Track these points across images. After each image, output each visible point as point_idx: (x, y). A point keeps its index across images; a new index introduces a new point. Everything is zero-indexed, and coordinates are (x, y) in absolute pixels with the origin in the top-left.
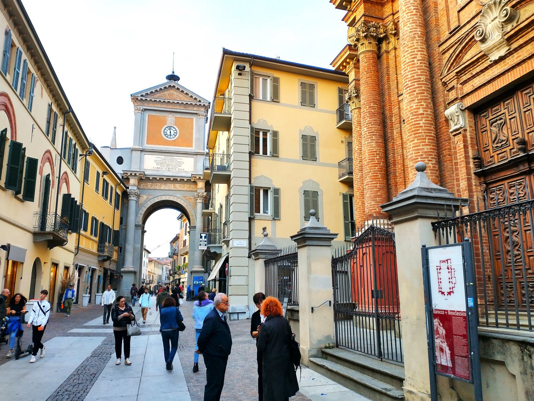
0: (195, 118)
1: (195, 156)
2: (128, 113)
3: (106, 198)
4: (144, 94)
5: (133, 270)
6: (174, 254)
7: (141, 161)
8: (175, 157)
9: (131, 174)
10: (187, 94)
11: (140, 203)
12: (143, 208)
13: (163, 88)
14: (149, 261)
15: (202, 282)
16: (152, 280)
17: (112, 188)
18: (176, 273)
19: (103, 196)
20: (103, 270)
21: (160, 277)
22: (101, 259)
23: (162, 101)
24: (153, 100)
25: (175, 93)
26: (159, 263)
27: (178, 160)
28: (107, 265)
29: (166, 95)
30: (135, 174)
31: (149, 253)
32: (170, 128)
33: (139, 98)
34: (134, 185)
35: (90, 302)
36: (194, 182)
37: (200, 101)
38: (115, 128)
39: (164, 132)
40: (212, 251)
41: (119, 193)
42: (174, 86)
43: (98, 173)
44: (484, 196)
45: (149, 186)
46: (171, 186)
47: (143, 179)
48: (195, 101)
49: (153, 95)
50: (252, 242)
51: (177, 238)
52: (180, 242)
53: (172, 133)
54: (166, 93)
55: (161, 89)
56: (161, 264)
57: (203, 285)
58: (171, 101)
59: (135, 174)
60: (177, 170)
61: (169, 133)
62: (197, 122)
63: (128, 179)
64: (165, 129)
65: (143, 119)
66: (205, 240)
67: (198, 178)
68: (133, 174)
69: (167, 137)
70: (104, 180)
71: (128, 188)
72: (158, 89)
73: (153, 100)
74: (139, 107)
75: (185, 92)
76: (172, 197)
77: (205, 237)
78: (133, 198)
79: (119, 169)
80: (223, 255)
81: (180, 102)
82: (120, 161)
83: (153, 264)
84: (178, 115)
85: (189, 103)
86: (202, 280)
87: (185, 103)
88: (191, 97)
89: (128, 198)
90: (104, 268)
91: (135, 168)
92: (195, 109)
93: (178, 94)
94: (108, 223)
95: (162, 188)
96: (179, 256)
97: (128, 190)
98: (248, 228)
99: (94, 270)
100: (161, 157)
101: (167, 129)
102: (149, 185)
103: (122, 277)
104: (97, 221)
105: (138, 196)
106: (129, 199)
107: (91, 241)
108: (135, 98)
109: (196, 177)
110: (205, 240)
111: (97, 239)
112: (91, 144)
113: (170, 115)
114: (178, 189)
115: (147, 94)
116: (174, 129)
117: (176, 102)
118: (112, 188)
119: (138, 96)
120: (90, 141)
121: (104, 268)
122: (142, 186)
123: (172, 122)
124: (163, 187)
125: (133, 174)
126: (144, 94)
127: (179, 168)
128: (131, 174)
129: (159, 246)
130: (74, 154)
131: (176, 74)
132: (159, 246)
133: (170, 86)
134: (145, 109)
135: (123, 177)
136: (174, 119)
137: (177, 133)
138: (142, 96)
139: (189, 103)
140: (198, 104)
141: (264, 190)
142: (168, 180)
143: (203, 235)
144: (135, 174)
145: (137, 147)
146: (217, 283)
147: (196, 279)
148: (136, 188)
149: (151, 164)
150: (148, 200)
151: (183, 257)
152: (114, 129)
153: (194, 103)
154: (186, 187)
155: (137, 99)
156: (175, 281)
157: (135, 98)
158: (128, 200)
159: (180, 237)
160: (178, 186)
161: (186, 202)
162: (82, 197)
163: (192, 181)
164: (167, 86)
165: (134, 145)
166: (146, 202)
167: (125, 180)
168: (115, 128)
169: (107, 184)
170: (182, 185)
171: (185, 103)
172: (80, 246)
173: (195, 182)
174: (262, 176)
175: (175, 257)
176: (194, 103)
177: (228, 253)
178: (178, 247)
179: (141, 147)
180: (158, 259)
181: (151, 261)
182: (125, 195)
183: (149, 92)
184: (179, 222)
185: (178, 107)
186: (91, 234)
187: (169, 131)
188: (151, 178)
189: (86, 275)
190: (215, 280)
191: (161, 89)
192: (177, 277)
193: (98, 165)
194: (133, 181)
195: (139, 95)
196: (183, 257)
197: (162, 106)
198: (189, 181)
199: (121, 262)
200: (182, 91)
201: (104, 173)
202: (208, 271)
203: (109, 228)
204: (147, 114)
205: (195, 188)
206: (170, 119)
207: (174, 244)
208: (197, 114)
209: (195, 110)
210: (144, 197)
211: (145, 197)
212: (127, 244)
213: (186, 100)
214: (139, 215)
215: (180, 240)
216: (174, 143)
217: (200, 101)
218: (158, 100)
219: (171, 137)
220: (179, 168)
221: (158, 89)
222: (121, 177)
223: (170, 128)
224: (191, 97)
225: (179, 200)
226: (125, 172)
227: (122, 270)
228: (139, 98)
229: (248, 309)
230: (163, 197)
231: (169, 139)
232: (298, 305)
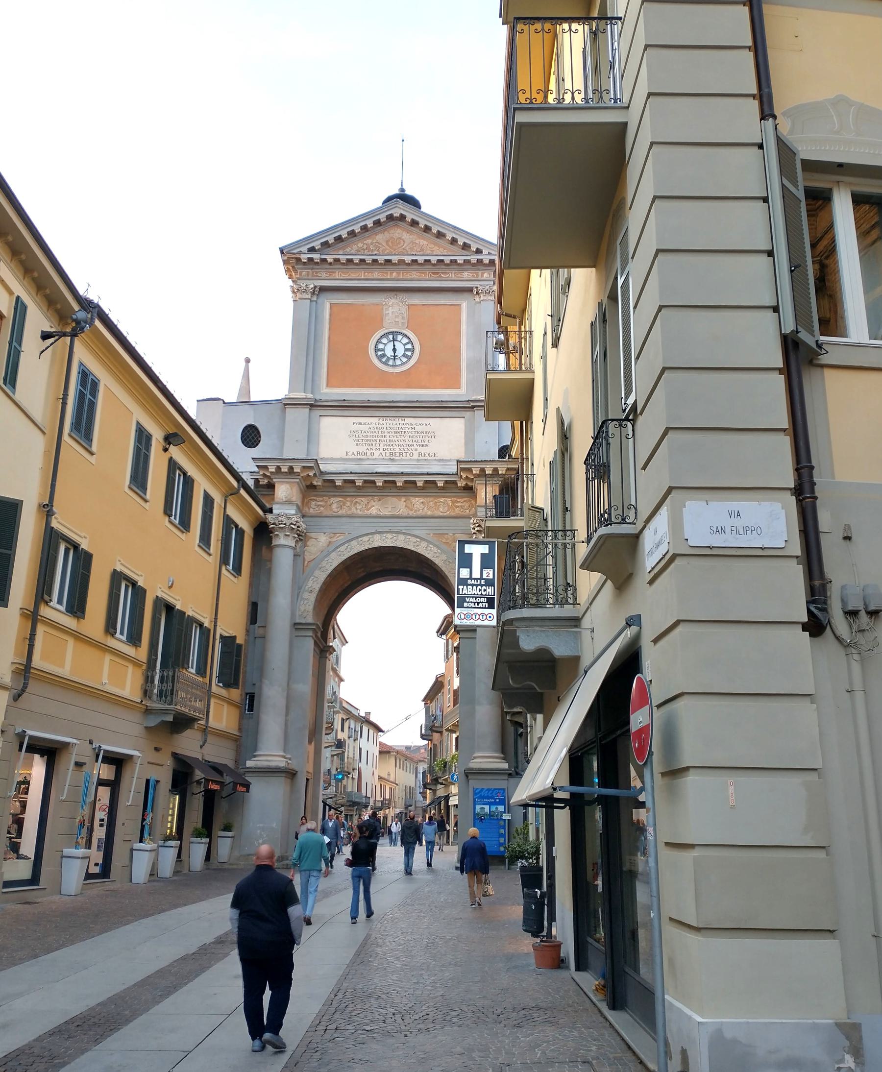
0: (464, 304)
1: (468, 414)
2: (275, 298)
3: (185, 524)
4: (317, 244)
5: (281, 763)
6: (431, 730)
7: (312, 436)
8: (408, 420)
10: (440, 235)
11: (308, 557)
12: (317, 573)
13: (370, 223)
14: (380, 752)
15: (501, 808)
16: (390, 800)
17: (208, 501)
18: (436, 781)
19: (168, 511)
20: (169, 763)
21: (410, 791)
22: (153, 721)
23: (369, 259)
24: (343, 258)
25: (406, 236)
26: (407, 758)
27: (419, 428)
28: (189, 744)
29: (380, 245)
30: (291, 468)
31: (379, 729)
32: (394, 335)
33: (304, 258)
34: (289, 503)
35: (208, 858)
37: (479, 251)
38: (248, 361)
39: (376, 350)
40: (528, 642)
41: (244, 524)
42: (402, 218)
43: (143, 438)
45: (334, 506)
46: (398, 505)
47: (317, 485)
48: (464, 252)
49: (343, 248)
50: (825, 519)
51: (438, 686)
52: (447, 697)
53: (400, 351)
54: (381, 237)
55: (365, 228)
56: (411, 760)
57: (506, 817)
58: (395, 259)
60: (416, 456)
61: (389, 352)
62: (471, 314)
63: (271, 486)
64: (379, 341)
65: (315, 318)
66: (488, 574)
67: (476, 471)
69: (386, 363)
70: (173, 465)
71: (270, 511)
72: (357, 229)
73: (343, 258)
74: (303, 284)
75: (434, 231)
76: (402, 537)
77: (486, 562)
78: (283, 541)
79: (244, 461)
80: (585, 662)
81: (421, 259)
82: (251, 436)
83: (393, 760)
84: (417, 300)
85: (447, 259)
86: (501, 802)
87: (434, 259)
88: (454, 241)
89: (271, 539)
90: (175, 755)
91: (294, 450)
92: (466, 275)
93: (413, 237)
94: (193, 604)
95: (374, 511)
96: (445, 733)
97: (270, 518)
98: (784, 422)
99: (118, 761)
100: (367, 423)
101: (384, 341)
102: (335, 504)
103: (247, 786)
104: (139, 593)
105: (302, 537)
106: (275, 542)
107: (108, 658)
108: (295, 259)
109: (469, 470)
110: (488, 574)
111: (142, 653)
112: (87, 305)
113: (392, 301)
114: (420, 513)
115: (326, 244)
116: (405, 340)
117: (408, 259)
118: (208, 501)
119: (300, 253)
120: (81, 291)
121: (175, 755)
122: (316, 506)
123: (399, 320)
124: (376, 508)
126: (317, 244)
127: (421, 450)
129: (407, 718)
131: (408, 192)
132: (407, 718)
133: (390, 218)
134: (323, 289)
135: (257, 481)
136: (404, 310)
137: (412, 350)
138: (312, 250)
139: (447, 259)
140: (474, 259)
141: (858, 200)
142: (390, 484)
143: (477, 551)
145: (301, 395)
146: (562, 818)
147: (480, 796)
148: (292, 511)
149: (340, 443)
150: (332, 548)
151: (454, 736)
152: (244, 363)
153: (460, 260)
154: (444, 505)
155: (298, 260)
156: (436, 802)
157: (295, 259)
158: (270, 547)
159: (446, 683)
160: (419, 504)
161: (443, 551)
162: (53, 486)
163: (459, 485)
164: (382, 217)
165: (291, 390)
166: (326, 553)
167: (262, 490)
168: (248, 361)
169: (189, 482)
170: (431, 501)
171: (434, 259)
172: (37, 661)
173: (469, 490)
174: (841, 102)
175: (436, 736)
176: (460, 260)
177: (633, 621)
178: (442, 711)
179: (310, 396)
180: (408, 748)
181: (385, 751)
182: (263, 532)
183: (331, 239)
184: (441, 642)
185: (415, 275)
186: (110, 627)
187: (390, 346)
188: (339, 483)
189: (84, 775)
190: (547, 802)
191: (365, 228)
192: (441, 792)
193: (143, 406)
194: (283, 490)
195: (304, 249)
196: (454, 736)
197: (370, 276)
198: (450, 485)
199: (245, 740)
200: (427, 229)
201: (170, 439)
202: (515, 750)
203: (201, 625)
204: (326, 303)
205: (470, 508)
206: (394, 310)
207: (433, 705)
208: (470, 290)
209: (465, 279)
210: (319, 541)
211: (323, 539)
212: (266, 682)
213: (436, 251)
214: (306, 595)
215: (445, 690)
216: (406, 379)
217: (479, 251)
218: (356, 259)
219: (398, 362)
220: (421, 450)
221: (357, 229)
222: (251, 483)
223: (394, 335)
224: (454, 241)
225: (424, 544)
226: (262, 464)
227: (249, 764)
228: (304, 258)
229: (857, 1052)
230: (377, 537)
231: (391, 370)
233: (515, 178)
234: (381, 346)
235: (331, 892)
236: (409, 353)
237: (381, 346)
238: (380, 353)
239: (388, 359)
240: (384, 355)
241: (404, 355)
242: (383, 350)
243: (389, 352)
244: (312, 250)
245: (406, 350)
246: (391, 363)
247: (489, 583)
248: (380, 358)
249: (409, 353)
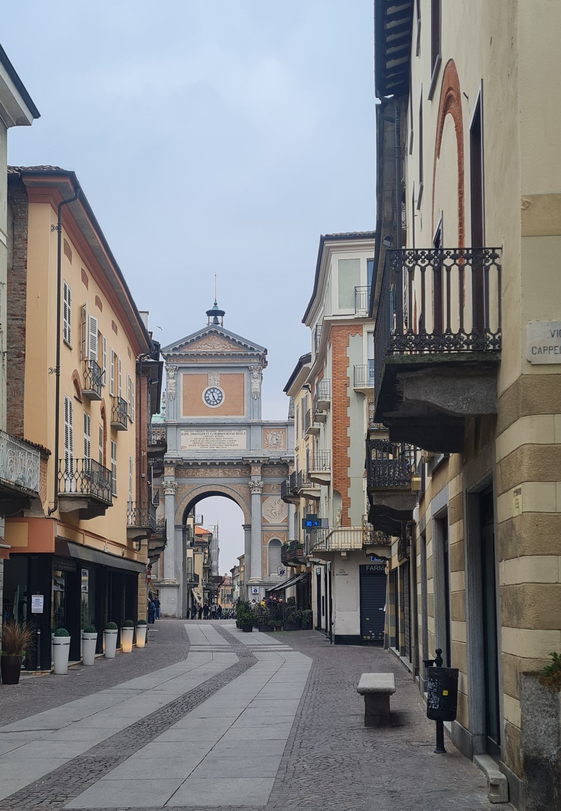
9: (253, 461)
24: (183, 354)
36: (247, 465)
37: (252, 349)
39: (205, 397)
44: (113, 455)
59: (259, 462)
64: (206, 393)
68: (256, 461)
73: (183, 354)
115: (181, 346)
116: (218, 392)
125: (256, 461)
128: (253, 461)
130: (105, 440)
136: (218, 378)
137: (222, 397)
138: (175, 349)
142: (204, 465)
144: (259, 462)
187: (211, 395)
213: (228, 349)
232: (192, 619)
233: (128, 333)
234: (207, 395)
235: (8, 624)
236: (220, 398)
237: (207, 395)
238: (207, 399)
239: (211, 401)
240: (209, 399)
241: (218, 399)
242: (208, 397)
243: (211, 398)
244: (175, 349)
245: (219, 397)
246: (212, 403)
247: (82, 491)
248: (207, 401)
249: (220, 398)
